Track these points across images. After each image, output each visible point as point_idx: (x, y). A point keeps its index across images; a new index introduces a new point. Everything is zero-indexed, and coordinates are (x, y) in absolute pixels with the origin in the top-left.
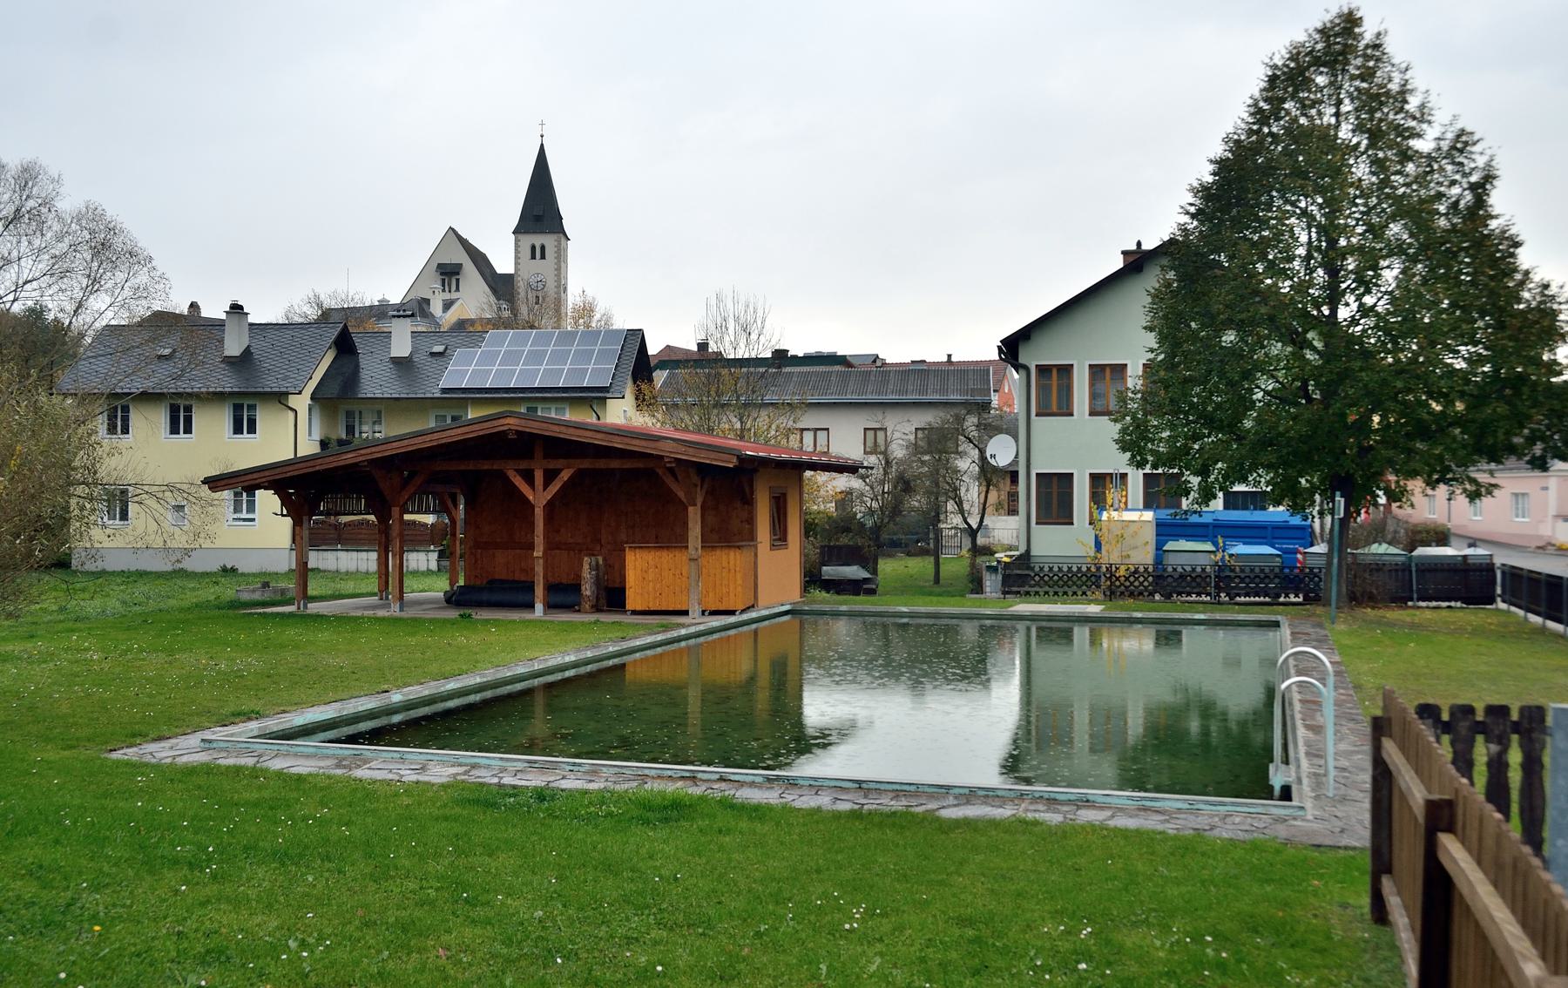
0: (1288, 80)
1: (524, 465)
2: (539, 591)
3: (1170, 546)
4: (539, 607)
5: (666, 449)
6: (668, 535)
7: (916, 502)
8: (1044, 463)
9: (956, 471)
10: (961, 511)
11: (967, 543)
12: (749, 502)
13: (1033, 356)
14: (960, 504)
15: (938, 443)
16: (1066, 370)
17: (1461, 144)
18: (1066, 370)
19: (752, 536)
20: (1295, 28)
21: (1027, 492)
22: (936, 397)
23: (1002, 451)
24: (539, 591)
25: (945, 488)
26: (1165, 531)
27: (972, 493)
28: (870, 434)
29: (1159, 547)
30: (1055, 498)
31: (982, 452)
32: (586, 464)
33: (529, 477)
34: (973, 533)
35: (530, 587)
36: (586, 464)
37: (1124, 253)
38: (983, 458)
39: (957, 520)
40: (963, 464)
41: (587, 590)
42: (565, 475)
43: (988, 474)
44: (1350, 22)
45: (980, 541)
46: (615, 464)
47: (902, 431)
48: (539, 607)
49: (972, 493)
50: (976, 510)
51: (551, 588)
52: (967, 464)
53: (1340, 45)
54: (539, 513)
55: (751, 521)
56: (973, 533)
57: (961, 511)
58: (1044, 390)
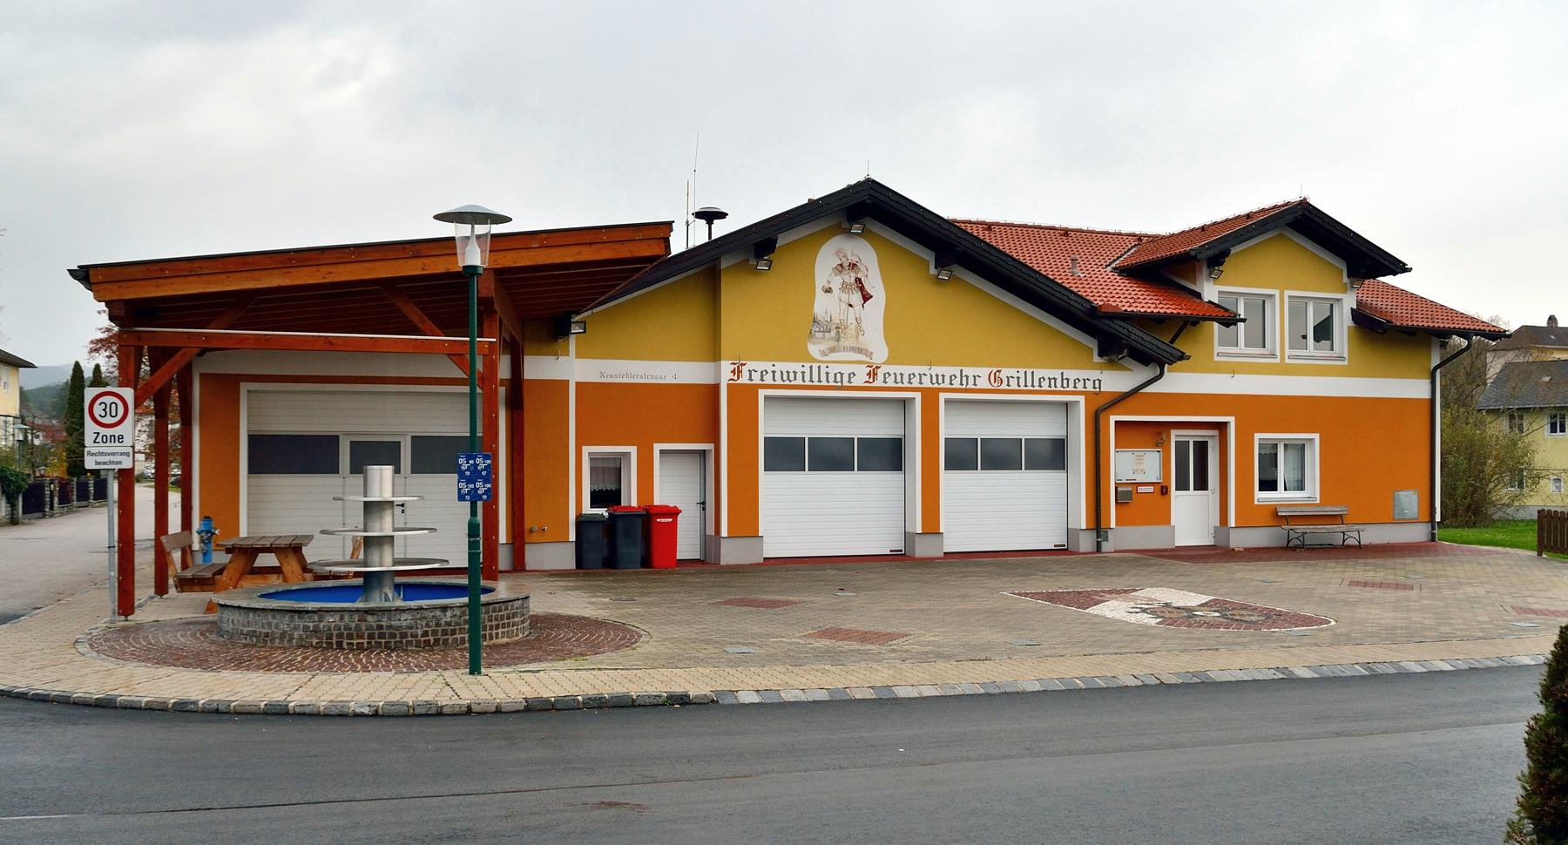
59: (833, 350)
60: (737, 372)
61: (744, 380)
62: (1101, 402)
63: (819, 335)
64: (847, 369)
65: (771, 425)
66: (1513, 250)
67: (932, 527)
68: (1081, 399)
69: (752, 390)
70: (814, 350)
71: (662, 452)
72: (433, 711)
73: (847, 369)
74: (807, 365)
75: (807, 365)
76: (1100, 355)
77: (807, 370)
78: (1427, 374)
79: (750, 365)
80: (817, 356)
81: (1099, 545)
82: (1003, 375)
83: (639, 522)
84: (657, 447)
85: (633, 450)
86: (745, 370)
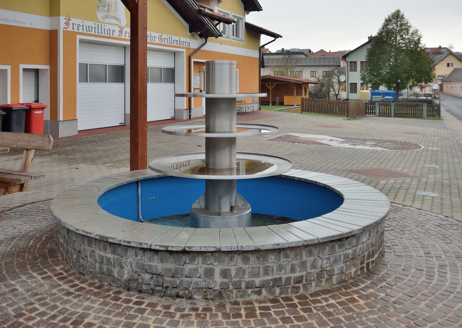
0: (388, 21)
1: (268, 83)
2: (271, 102)
3: (373, 96)
4: (271, 105)
5: (292, 81)
6: (291, 94)
7: (324, 88)
8: (351, 81)
9: (333, 82)
10: (334, 90)
11: (335, 98)
12: (301, 89)
13: (349, 59)
14: (334, 89)
15: (329, 75)
16: (356, 62)
17: (416, 31)
18: (356, 62)
19: (302, 94)
20: (393, 11)
21: (348, 88)
22: (328, 64)
23: (343, 78)
24: (271, 102)
25: (330, 85)
26: (373, 94)
27: (336, 87)
28: (312, 73)
29: (371, 96)
30: (353, 88)
31: (339, 78)
32: (278, 83)
33: (269, 85)
34: (337, 95)
35: (269, 102)
36: (278, 83)
37: (369, 37)
38: (339, 79)
39: (333, 92)
40: (334, 80)
41: (277, 102)
42: (275, 85)
43: (340, 83)
44: (398, 11)
45: (338, 97)
46: (283, 83)
47: (320, 73)
48: (271, 105)
49: (336, 87)
50: (337, 90)
51: (272, 102)
52: (335, 80)
53: (397, 16)
54: (271, 90)
55: (302, 92)
56: (337, 95)
57: (334, 90)
58: (351, 66)
59: (107, 17)
60: (67, 24)
61: (70, 29)
62: (191, 52)
63: (101, 8)
64: (112, 27)
65: (84, 57)
66: (460, 48)
67: (37, 101)
68: (184, 50)
69: (74, 34)
70: (100, 15)
71: (25, 70)
72: (112, 245)
73: (112, 27)
74: (97, 24)
75: (97, 24)
76: (190, 32)
77: (96, 26)
78: (258, 49)
79: (73, 21)
80: (101, 20)
81: (190, 116)
82: (163, 37)
83: (24, 114)
84: (22, 66)
85: (8, 68)
86: (71, 22)
